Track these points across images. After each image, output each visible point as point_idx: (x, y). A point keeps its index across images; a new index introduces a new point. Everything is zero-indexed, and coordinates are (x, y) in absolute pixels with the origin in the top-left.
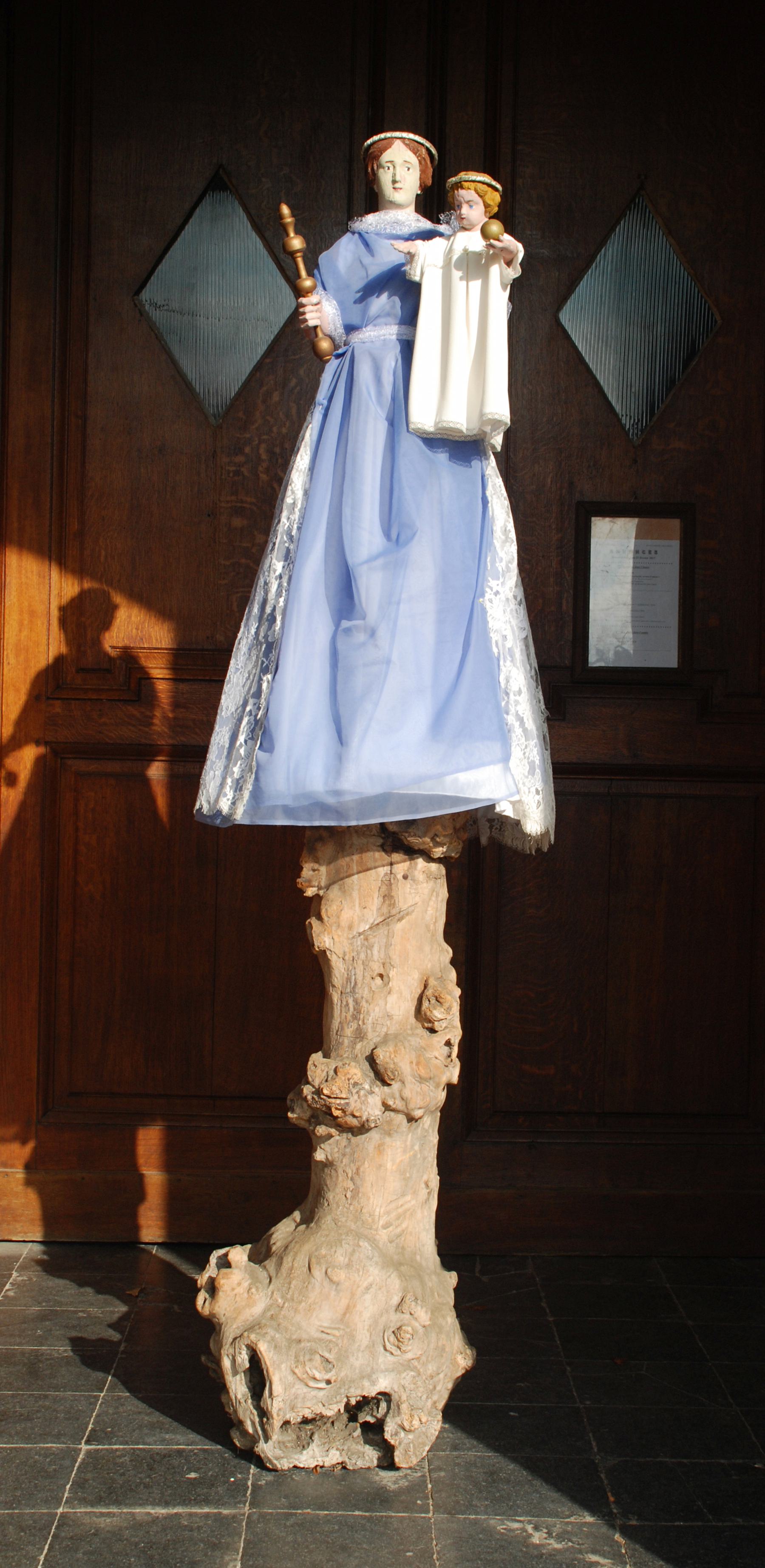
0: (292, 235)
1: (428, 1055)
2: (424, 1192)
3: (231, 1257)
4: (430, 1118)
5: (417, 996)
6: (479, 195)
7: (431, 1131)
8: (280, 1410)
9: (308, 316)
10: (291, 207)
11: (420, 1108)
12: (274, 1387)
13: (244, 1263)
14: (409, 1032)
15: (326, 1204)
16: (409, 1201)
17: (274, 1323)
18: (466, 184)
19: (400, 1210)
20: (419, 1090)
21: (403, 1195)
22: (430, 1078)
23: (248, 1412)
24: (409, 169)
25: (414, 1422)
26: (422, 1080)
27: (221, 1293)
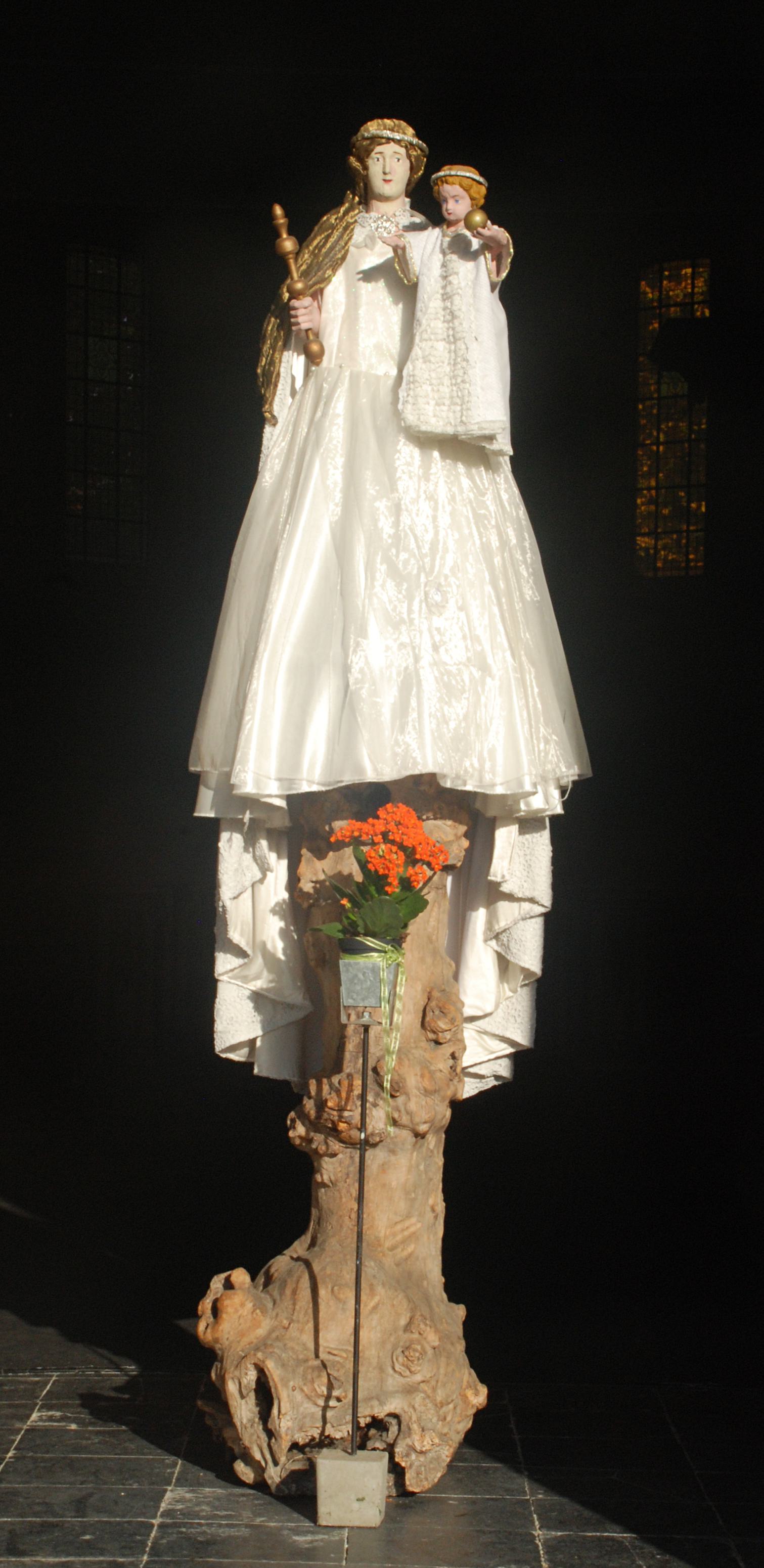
0: (285, 236)
1: (433, 1068)
2: (430, 1215)
3: (233, 1279)
4: (434, 1139)
5: (422, 1009)
6: (465, 190)
7: (435, 1152)
8: (288, 1428)
9: (300, 319)
10: (284, 207)
11: (425, 1123)
12: (282, 1404)
13: (247, 1286)
14: (413, 1045)
15: (330, 1228)
16: (415, 1224)
17: (280, 1344)
18: (450, 179)
19: (406, 1233)
20: (424, 1103)
21: (408, 1216)
22: (435, 1091)
23: (255, 1437)
24: (399, 160)
25: (425, 1443)
26: (427, 1093)
27: (224, 1316)
